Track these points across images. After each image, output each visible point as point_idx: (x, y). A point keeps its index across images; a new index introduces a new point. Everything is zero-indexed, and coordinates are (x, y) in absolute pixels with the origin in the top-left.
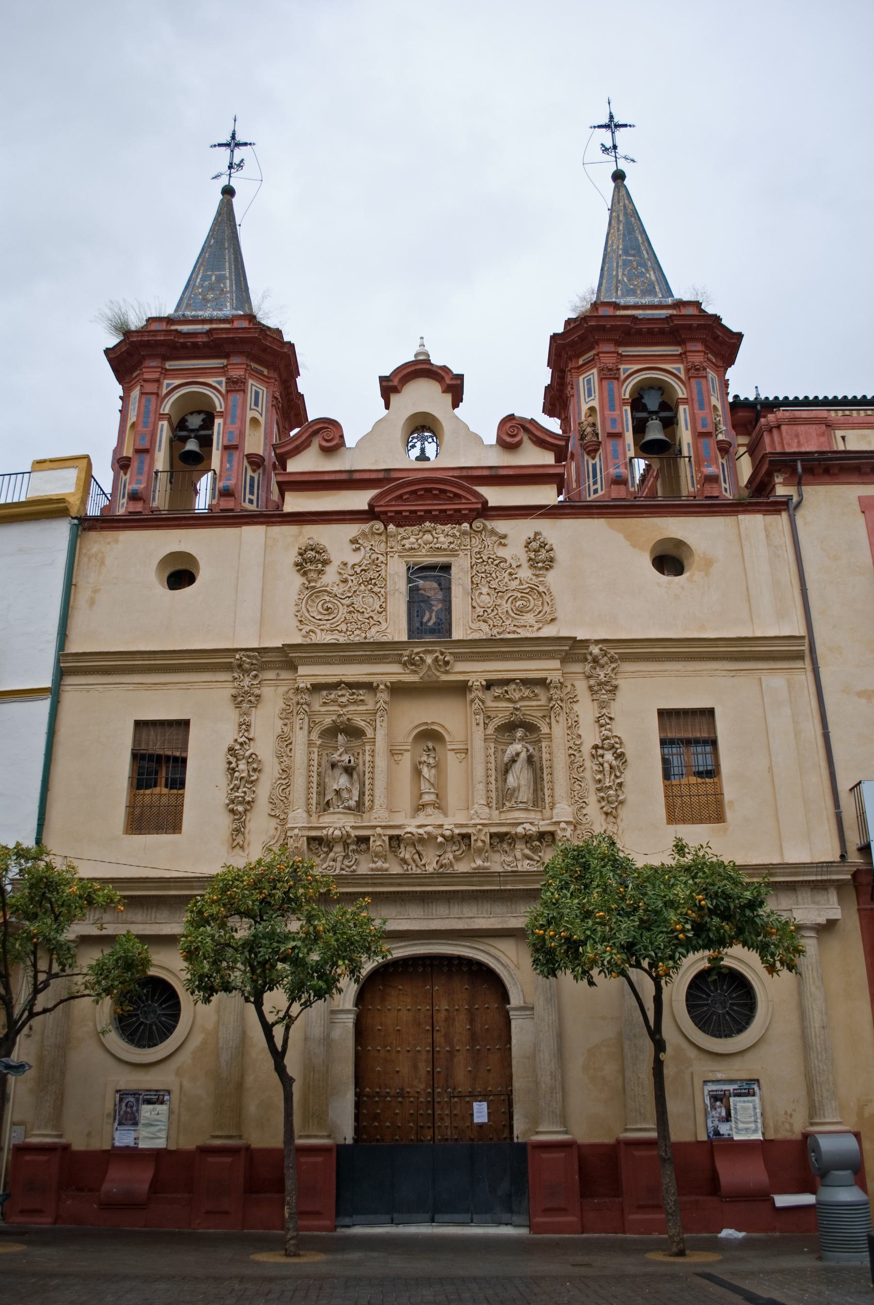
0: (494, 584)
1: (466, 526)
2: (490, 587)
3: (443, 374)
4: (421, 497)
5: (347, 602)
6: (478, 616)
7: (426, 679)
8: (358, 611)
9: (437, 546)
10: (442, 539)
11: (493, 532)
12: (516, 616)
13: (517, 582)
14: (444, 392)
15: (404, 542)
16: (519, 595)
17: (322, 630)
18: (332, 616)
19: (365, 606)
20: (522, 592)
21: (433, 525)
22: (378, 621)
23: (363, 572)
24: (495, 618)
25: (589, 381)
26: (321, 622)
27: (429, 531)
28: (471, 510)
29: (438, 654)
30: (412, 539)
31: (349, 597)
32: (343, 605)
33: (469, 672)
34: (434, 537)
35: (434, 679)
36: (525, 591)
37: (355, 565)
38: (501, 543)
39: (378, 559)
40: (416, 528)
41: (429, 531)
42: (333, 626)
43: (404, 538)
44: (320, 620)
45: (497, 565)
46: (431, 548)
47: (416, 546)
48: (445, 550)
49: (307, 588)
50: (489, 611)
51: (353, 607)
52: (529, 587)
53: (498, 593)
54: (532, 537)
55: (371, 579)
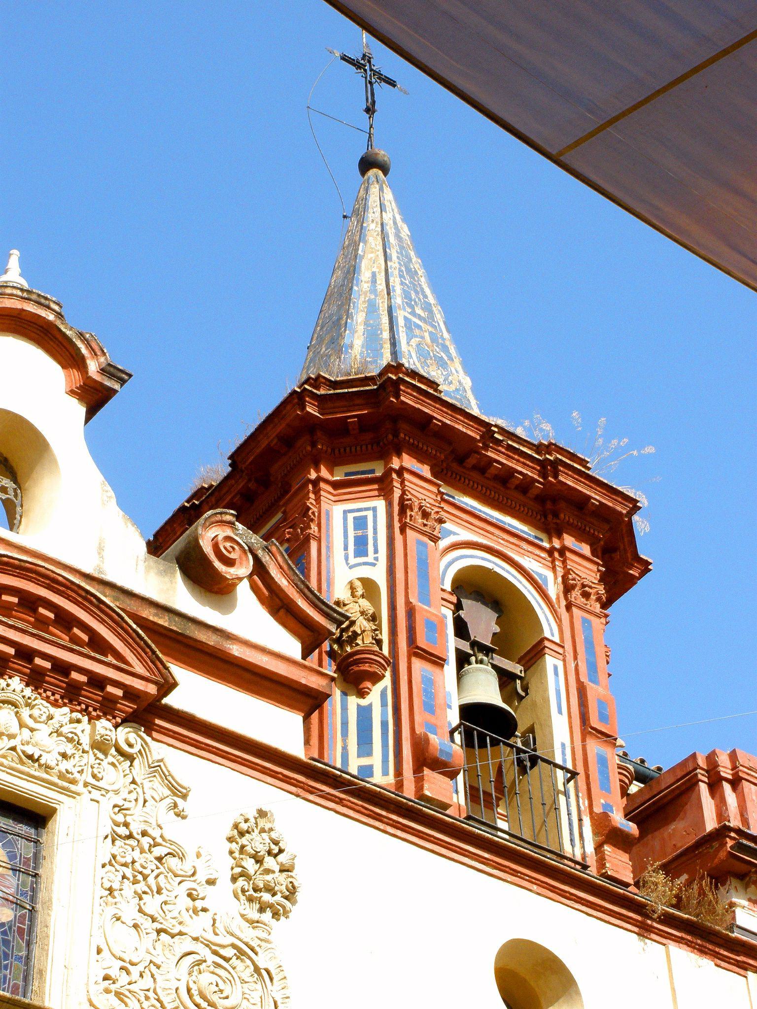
0: (152, 904)
1: (104, 726)
2: (140, 911)
3: (84, 351)
6: (106, 978)
9: (30, 750)
11: (157, 769)
13: (205, 919)
14: (72, 392)
20: (215, 953)
21: (28, 692)
24: (147, 998)
25: (360, 523)
27: (14, 704)
28: (130, 694)
34: (22, 725)
36: (222, 952)
38: (175, 805)
41: (14, 704)
45: (160, 859)
46: (13, 749)
48: (47, 768)
50: (135, 975)
52: (234, 946)
54: (252, 814)
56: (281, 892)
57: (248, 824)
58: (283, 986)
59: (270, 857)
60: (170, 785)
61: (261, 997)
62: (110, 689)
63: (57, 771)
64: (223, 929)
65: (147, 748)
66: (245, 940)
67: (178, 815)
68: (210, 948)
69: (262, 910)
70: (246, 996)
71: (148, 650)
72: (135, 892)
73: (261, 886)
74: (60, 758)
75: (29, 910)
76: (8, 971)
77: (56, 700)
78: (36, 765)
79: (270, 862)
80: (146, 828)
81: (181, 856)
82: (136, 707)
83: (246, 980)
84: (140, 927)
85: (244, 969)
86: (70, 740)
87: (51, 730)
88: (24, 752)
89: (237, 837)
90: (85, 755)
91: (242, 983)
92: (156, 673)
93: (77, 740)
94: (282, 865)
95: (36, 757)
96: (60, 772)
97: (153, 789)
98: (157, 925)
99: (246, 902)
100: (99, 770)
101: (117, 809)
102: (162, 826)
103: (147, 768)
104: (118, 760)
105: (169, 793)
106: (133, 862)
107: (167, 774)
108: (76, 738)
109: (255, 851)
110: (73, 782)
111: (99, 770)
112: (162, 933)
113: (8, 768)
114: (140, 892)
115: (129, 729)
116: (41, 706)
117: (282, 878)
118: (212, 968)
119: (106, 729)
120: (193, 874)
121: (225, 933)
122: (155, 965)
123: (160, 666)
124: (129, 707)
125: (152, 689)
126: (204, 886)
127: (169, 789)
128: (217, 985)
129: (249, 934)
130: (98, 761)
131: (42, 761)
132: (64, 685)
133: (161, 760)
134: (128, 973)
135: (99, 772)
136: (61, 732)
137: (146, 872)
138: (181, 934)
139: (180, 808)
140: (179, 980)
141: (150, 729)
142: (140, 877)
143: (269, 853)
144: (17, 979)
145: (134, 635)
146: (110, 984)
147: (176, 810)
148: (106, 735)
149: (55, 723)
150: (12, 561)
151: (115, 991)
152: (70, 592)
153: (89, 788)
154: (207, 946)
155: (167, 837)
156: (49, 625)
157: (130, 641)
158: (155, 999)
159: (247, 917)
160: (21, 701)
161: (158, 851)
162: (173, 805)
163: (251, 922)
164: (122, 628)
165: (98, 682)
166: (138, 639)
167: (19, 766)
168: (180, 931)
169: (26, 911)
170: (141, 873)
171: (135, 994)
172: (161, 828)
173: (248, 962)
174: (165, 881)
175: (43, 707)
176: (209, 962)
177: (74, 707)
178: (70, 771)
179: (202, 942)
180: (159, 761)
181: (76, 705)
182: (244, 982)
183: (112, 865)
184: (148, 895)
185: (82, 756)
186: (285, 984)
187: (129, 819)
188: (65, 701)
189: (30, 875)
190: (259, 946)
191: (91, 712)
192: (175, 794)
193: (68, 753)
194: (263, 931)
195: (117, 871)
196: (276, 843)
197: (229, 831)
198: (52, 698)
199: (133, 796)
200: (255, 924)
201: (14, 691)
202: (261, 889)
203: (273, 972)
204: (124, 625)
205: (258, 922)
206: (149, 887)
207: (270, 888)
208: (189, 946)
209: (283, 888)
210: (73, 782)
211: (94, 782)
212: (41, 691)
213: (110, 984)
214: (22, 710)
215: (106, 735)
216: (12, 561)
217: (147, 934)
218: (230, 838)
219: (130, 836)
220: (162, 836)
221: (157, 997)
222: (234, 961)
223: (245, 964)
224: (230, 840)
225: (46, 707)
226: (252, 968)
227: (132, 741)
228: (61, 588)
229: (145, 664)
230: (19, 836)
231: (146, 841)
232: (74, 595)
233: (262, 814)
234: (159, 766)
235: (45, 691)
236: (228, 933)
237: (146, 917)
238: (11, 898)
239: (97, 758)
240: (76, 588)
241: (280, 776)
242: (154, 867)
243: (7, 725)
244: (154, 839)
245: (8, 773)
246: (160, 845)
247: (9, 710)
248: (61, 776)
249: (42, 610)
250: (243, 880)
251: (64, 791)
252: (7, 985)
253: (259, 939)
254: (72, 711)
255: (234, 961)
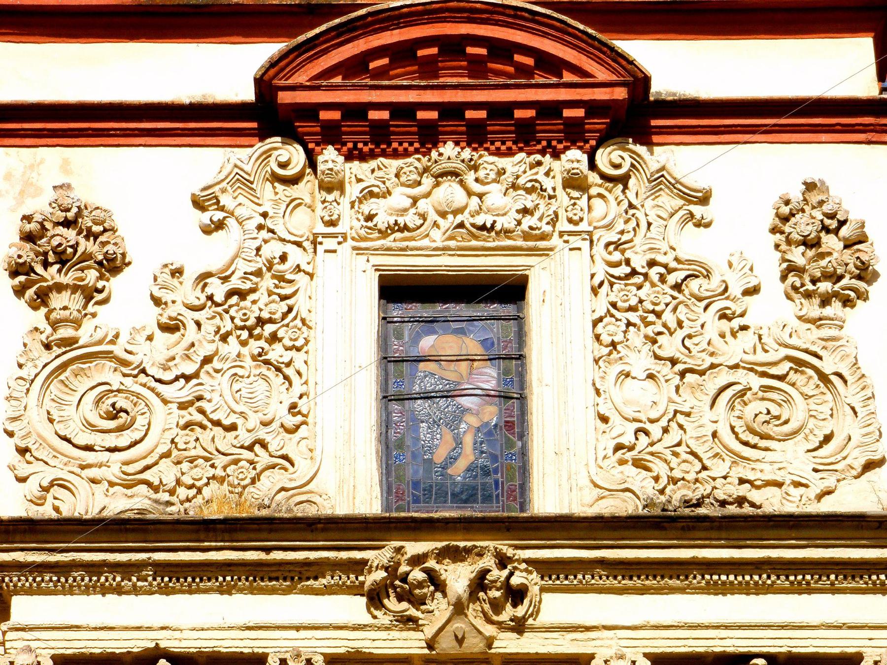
0: (670, 346)
2: (657, 357)
4: (429, 68)
5: (178, 392)
6: (618, 447)
7: (447, 645)
8: (217, 423)
9: (479, 220)
10: (495, 196)
12: (747, 452)
13: (747, 339)
15: (367, 207)
16: (756, 382)
17: (94, 481)
18: (124, 440)
19: (238, 408)
20: (764, 375)
21: (467, 153)
22: (285, 457)
23: (234, 299)
24: (676, 455)
26: (89, 457)
27: (455, 174)
28: (594, 108)
29: (488, 561)
30: (400, 198)
31: (187, 378)
32: (165, 402)
33: (588, 629)
34: (470, 194)
35: (474, 645)
36: (773, 371)
37: (209, 275)
38: (692, 215)
39: (283, 258)
40: (414, 162)
41: (455, 174)
42: (130, 469)
43: (372, 194)
44: (89, 448)
45: (677, 287)
46: (461, 225)
47: (411, 219)
48: (507, 233)
49: (48, 347)
51: (202, 411)
52: (788, 358)
53: (682, 374)
55: (261, 322)
56: (850, 273)
57: (790, 206)
58: (861, 386)
59: (829, 235)
60: (681, 194)
61: (832, 410)
62: (567, 113)
63: (519, 233)
64: (773, 342)
65: (642, 163)
66: (804, 346)
67: (698, 225)
68: (756, 372)
69: (825, 302)
70: (812, 413)
71: (605, 49)
72: (646, 337)
73: (819, 274)
74: (519, 216)
75: (517, 398)
76: (499, 475)
77: (509, 149)
78: (493, 234)
79: (830, 242)
80: (653, 257)
81: (705, 273)
82: (608, 121)
83: (810, 394)
84: (656, 376)
85: (807, 381)
86: (529, 191)
87: (505, 186)
88: (473, 225)
89: (780, 225)
90: (553, 200)
91: (806, 399)
92: (623, 72)
93: (539, 187)
94: (845, 239)
95: (489, 225)
96: (523, 232)
97: (658, 206)
98: (679, 367)
99: (803, 300)
100: (575, 211)
101: (611, 248)
102: (674, 246)
103: (647, 184)
104: (606, 189)
105: (682, 202)
106: (641, 301)
107: (673, 181)
108: (537, 185)
109: (803, 236)
110: (544, 237)
111: (575, 211)
112: (687, 375)
113: (457, 250)
114: (652, 335)
115: (609, 149)
116: (485, 165)
117: (848, 256)
118: (760, 394)
119: (573, 162)
120: (726, 289)
121: (776, 347)
122: (682, 413)
123: (624, 63)
124: (599, 123)
125: (621, 93)
126: (740, 300)
127: (682, 198)
128: (769, 412)
129: (809, 337)
130: (573, 201)
131: (498, 227)
132: (513, 128)
133: (663, 168)
134: (647, 433)
135: (575, 215)
136: (518, 185)
137: (657, 308)
138: (713, 366)
139: (698, 216)
140: (716, 422)
141: (645, 138)
142: (651, 318)
143: (826, 229)
144: (512, 480)
145: (585, 37)
146: (623, 454)
147: (694, 221)
148: (573, 169)
149: (509, 177)
150: (413, 9)
151: (633, 459)
152: (497, 17)
153: (566, 237)
154: (751, 370)
155: (683, 256)
156: (486, 63)
157: (583, 45)
158: (687, 453)
159: (806, 317)
160: (462, 166)
161: (672, 279)
162: (689, 216)
163: (816, 322)
164: (570, 34)
165: (549, 110)
166: (590, 41)
167: (474, 243)
168: (712, 363)
169: (512, 401)
170: (653, 312)
171: (660, 455)
172: (674, 250)
173: (810, 372)
174: (686, 310)
175: (489, 162)
176: (755, 389)
177: (534, 148)
178: (535, 226)
179: (744, 368)
180: (658, 171)
181: (535, 145)
182: (807, 397)
183: (612, 316)
184: (664, 336)
185: (549, 204)
186: (865, 383)
187: (628, 254)
188: (519, 145)
189: (513, 358)
190: (824, 348)
191: (555, 147)
192: (690, 202)
193: (528, 207)
194: (830, 328)
195: (617, 320)
196: (832, 216)
197: (770, 219)
198: (503, 148)
199: (633, 223)
200: (818, 323)
201: (449, 158)
202: (820, 278)
203: (846, 374)
204: (570, 30)
205: (820, 319)
206: (665, 325)
207: (829, 274)
208: (723, 377)
209: (851, 267)
210: (544, 237)
211: (571, 228)
212: (488, 145)
213: (623, 454)
214: (466, 177)
215: (573, 169)
216: (413, 9)
217: (667, 381)
218: (773, 229)
219: (634, 273)
220: (676, 259)
221: (689, 450)
222: (792, 376)
223: (806, 376)
224: (774, 230)
225: (492, 164)
226: (816, 377)
227: (618, 161)
228: (484, 16)
229: (608, 67)
230: (494, 319)
231: (654, 272)
232: (501, 18)
233: (810, 187)
234: (663, 176)
235: (492, 143)
236: (780, 345)
237: (663, 362)
238: (493, 393)
239: (572, 198)
240: (501, 9)
241: (838, 127)
242: (669, 299)
243: (448, 202)
244: (665, 266)
245: (459, 255)
246: (675, 270)
247: (450, 183)
248: (526, 236)
249: (470, 50)
250: (793, 276)
251: (533, 251)
252: (500, 491)
253: (823, 339)
254: (529, 154)
255: (792, 376)
